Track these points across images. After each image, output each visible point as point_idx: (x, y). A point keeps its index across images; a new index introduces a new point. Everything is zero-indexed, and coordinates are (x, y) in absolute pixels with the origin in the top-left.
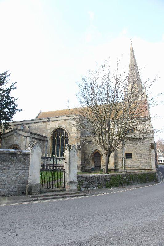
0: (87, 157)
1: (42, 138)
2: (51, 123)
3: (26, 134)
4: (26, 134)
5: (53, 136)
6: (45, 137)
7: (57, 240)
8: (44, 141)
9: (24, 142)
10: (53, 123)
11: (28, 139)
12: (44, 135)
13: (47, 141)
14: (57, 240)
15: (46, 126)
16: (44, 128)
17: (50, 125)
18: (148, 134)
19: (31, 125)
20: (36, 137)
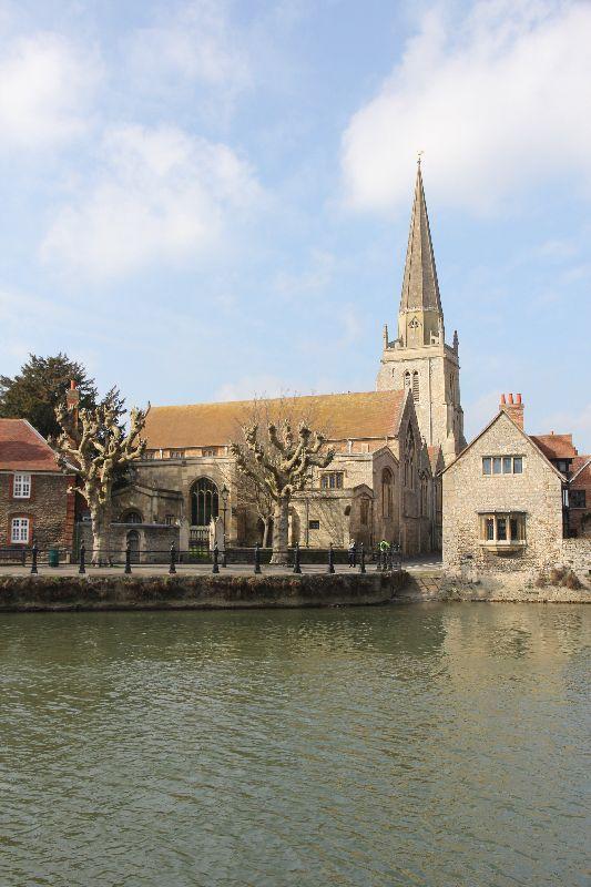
0: (250, 526)
1: (175, 496)
2: (188, 468)
3: (151, 493)
4: (151, 493)
5: (191, 491)
6: (179, 493)
7: (322, 694)
8: (177, 500)
9: (149, 505)
10: (192, 467)
11: (155, 500)
12: (176, 489)
13: (182, 500)
14: (322, 694)
15: (179, 472)
16: (175, 477)
17: (186, 471)
18: (214, 714)
19: (154, 469)
20: (165, 495)
